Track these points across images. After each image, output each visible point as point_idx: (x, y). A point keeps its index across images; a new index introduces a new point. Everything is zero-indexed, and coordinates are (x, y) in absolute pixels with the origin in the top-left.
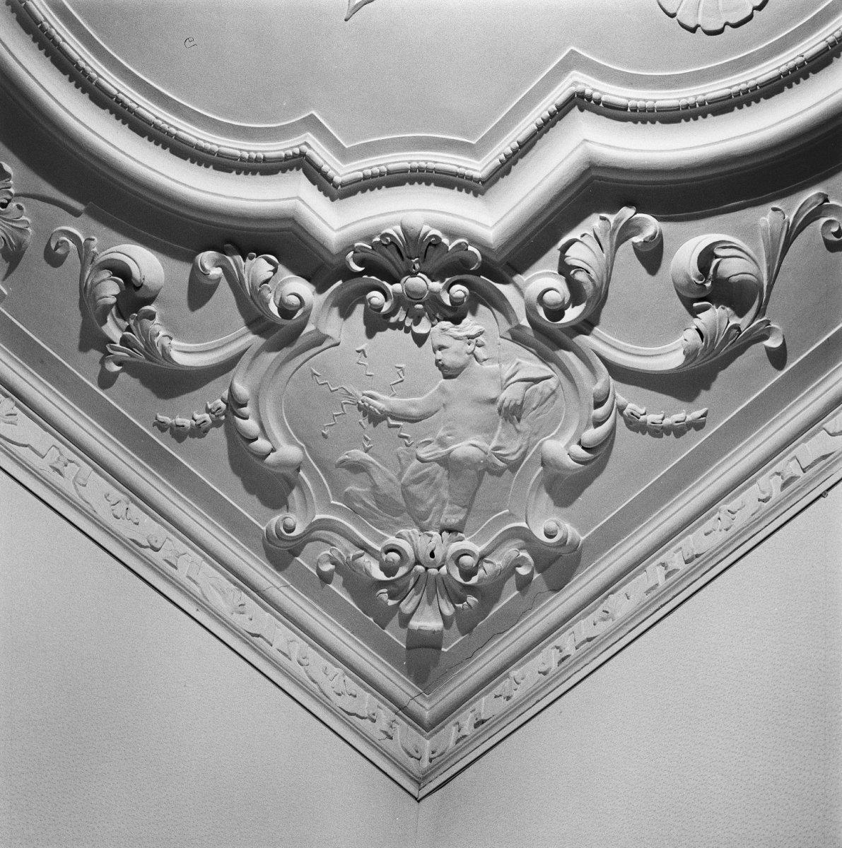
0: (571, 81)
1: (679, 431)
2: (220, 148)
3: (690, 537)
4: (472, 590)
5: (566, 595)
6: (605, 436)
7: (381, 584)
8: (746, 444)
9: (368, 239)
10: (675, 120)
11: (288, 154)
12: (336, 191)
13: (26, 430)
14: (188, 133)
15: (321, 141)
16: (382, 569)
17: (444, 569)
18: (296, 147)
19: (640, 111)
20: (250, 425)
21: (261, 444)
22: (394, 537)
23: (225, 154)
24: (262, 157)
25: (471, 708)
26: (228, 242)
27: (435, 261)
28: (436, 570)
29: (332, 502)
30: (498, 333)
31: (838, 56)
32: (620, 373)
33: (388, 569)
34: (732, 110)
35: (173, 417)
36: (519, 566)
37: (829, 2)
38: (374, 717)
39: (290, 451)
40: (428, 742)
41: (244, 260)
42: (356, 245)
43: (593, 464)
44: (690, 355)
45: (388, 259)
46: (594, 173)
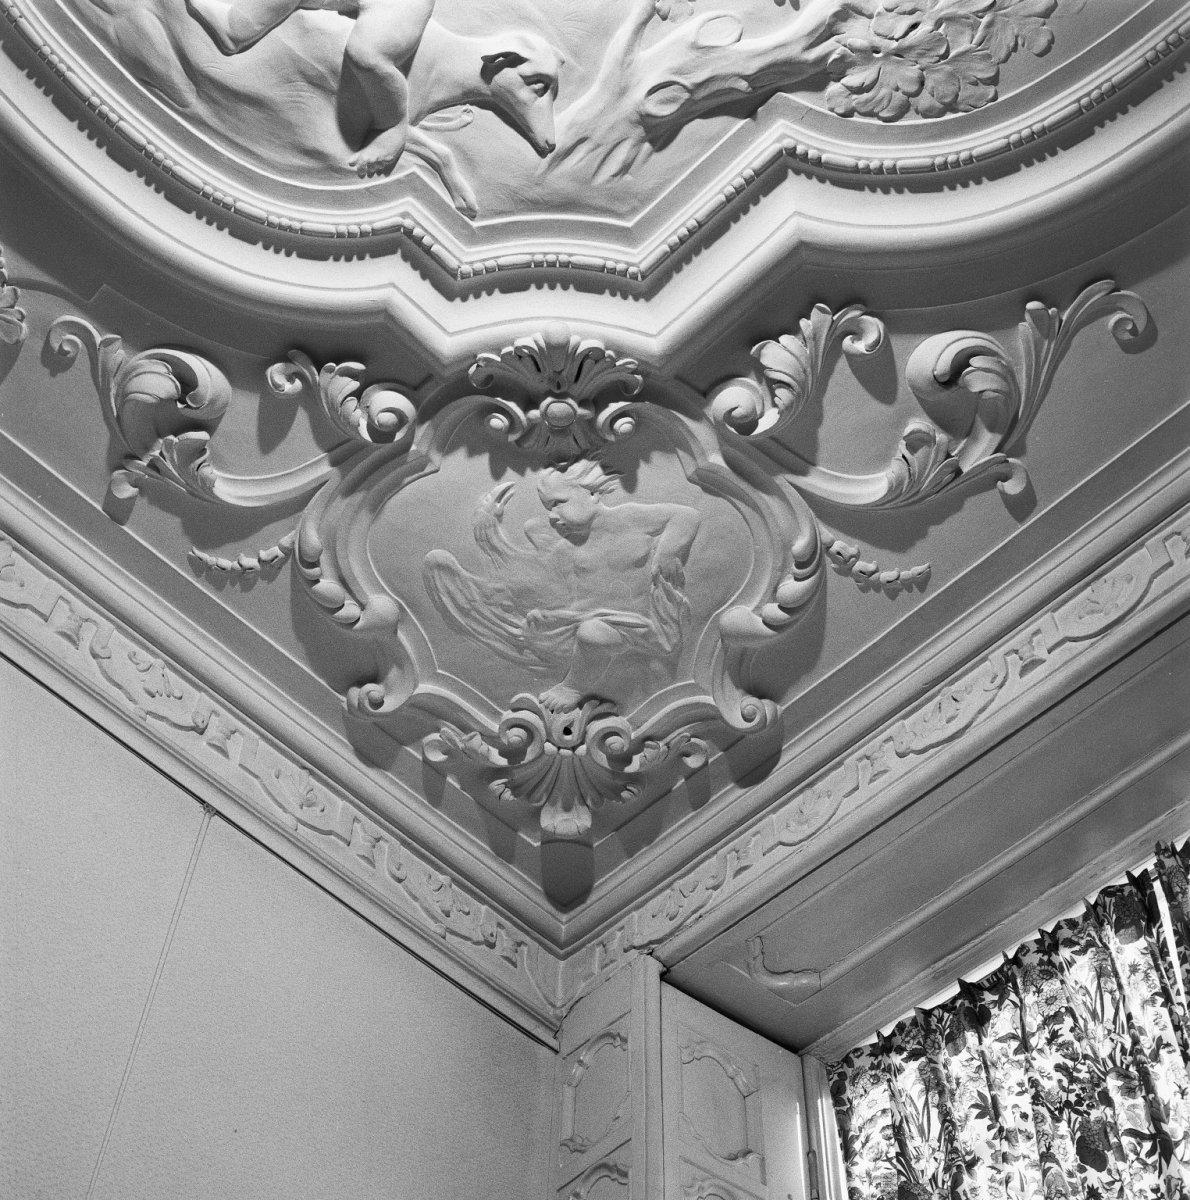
0: (402, 210)
1: (893, 589)
2: (304, 224)
3: (773, 816)
4: (635, 779)
5: (707, 815)
6: (804, 595)
7: (498, 772)
8: (1119, 505)
9: (497, 349)
10: (858, 186)
11: (681, 235)
12: (451, 285)
13: (41, 587)
14: (824, 1129)
15: (715, 176)
16: (502, 754)
17: (582, 750)
18: (719, 193)
19: (1015, 147)
20: (328, 585)
21: (350, 609)
22: (510, 711)
23: (385, 228)
24: (695, 224)
25: (619, 924)
26: (293, 348)
27: (590, 384)
28: (570, 752)
29: (440, 671)
30: (682, 474)
31: (1183, 70)
32: (825, 510)
33: (514, 753)
34: (254, 242)
35: (235, 557)
36: (688, 755)
37: (1150, 3)
38: (492, 940)
39: (382, 604)
40: (562, 963)
41: (319, 373)
42: (479, 356)
43: (789, 631)
44: (895, 490)
45: (531, 380)
46: (804, 253)
